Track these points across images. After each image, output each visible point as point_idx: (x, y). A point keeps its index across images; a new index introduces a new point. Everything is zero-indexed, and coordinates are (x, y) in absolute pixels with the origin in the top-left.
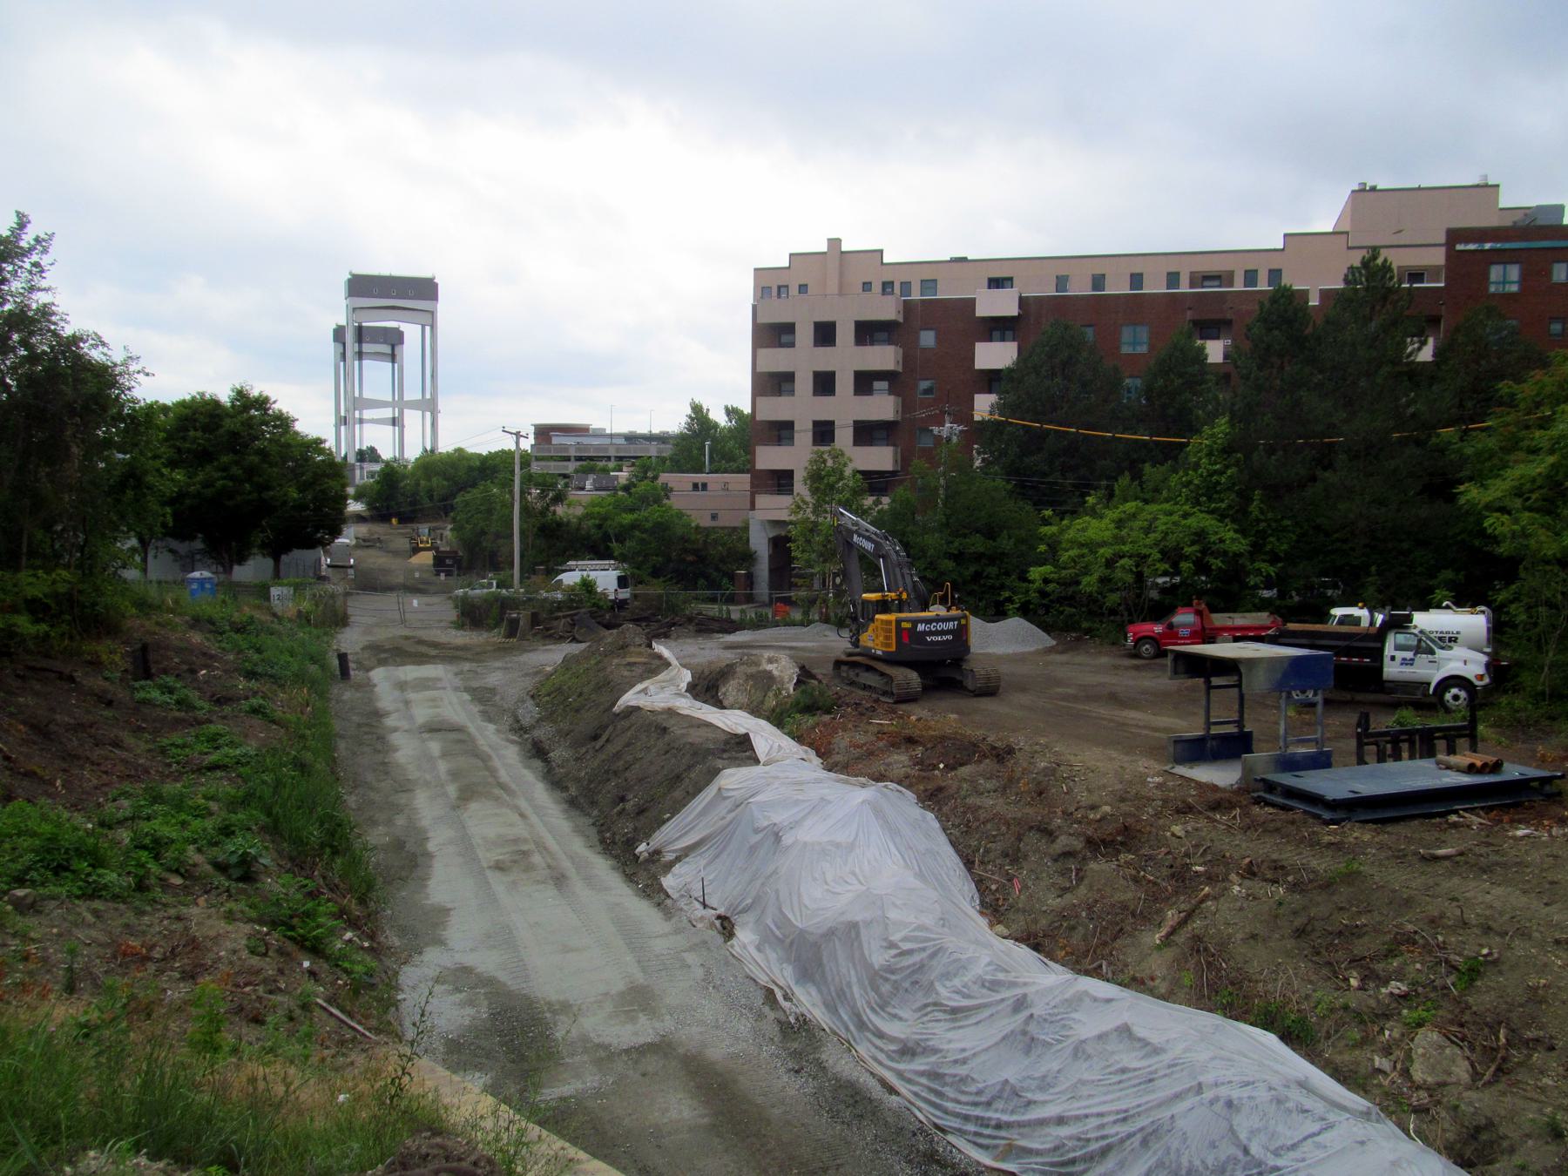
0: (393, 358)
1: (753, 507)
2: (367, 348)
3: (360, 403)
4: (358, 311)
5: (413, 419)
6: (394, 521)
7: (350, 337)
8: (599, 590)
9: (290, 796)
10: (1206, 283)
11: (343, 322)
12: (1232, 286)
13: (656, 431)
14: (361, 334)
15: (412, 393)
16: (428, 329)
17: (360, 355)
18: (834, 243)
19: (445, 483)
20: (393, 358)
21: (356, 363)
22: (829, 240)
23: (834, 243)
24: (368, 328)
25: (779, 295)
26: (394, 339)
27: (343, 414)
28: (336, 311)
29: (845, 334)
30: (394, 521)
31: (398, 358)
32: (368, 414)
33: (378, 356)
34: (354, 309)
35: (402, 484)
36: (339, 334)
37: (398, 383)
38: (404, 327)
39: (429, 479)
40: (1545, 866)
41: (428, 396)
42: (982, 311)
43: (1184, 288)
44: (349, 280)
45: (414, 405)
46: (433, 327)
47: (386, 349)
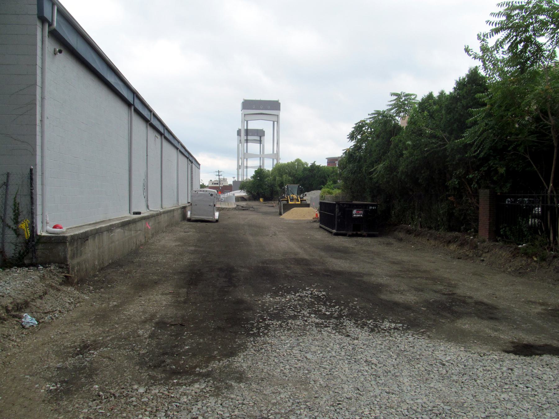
0: (260, 142)
2: (249, 138)
4: (246, 116)
6: (261, 200)
7: (243, 133)
9: (474, 216)
11: (240, 128)
14: (247, 132)
16: (276, 123)
17: (247, 141)
19: (290, 178)
20: (260, 142)
21: (245, 144)
26: (260, 134)
30: (261, 200)
31: (262, 142)
33: (254, 141)
35: (266, 179)
36: (239, 133)
37: (262, 150)
39: (281, 176)
40: (414, 412)
41: (275, 152)
44: (243, 102)
46: (278, 122)
47: (258, 138)
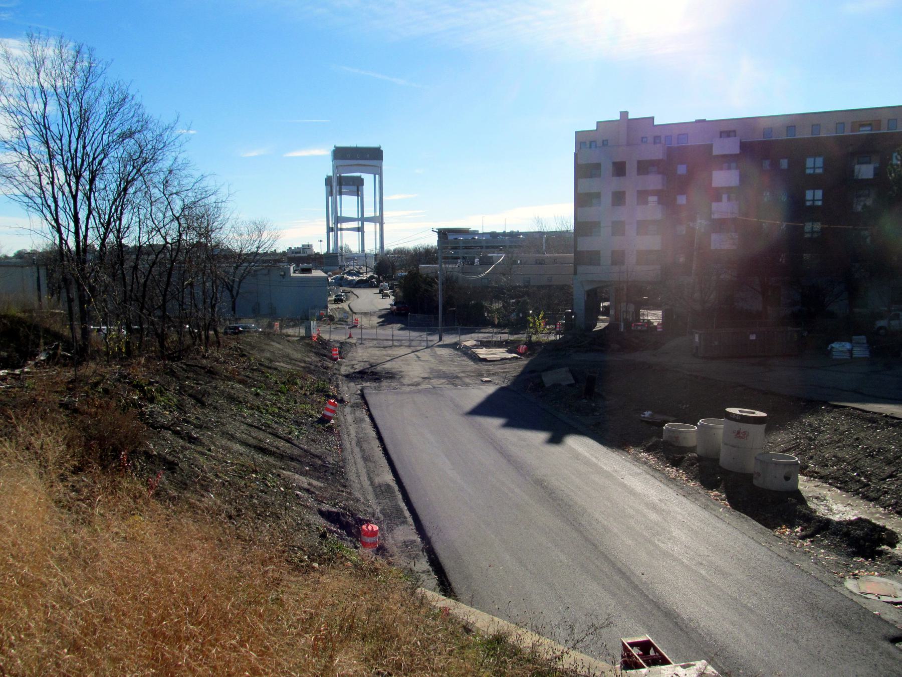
1: (575, 273)
3: (339, 219)
5: (369, 227)
8: (734, 247)
10: (861, 129)
12: (880, 130)
13: (508, 231)
15: (369, 212)
16: (377, 176)
18: (624, 114)
22: (621, 112)
23: (624, 114)
24: (344, 177)
25: (590, 147)
27: (331, 226)
28: (328, 169)
29: (632, 169)
32: (345, 225)
34: (337, 167)
36: (328, 181)
38: (364, 176)
42: (716, 151)
43: (848, 132)
45: (370, 220)
